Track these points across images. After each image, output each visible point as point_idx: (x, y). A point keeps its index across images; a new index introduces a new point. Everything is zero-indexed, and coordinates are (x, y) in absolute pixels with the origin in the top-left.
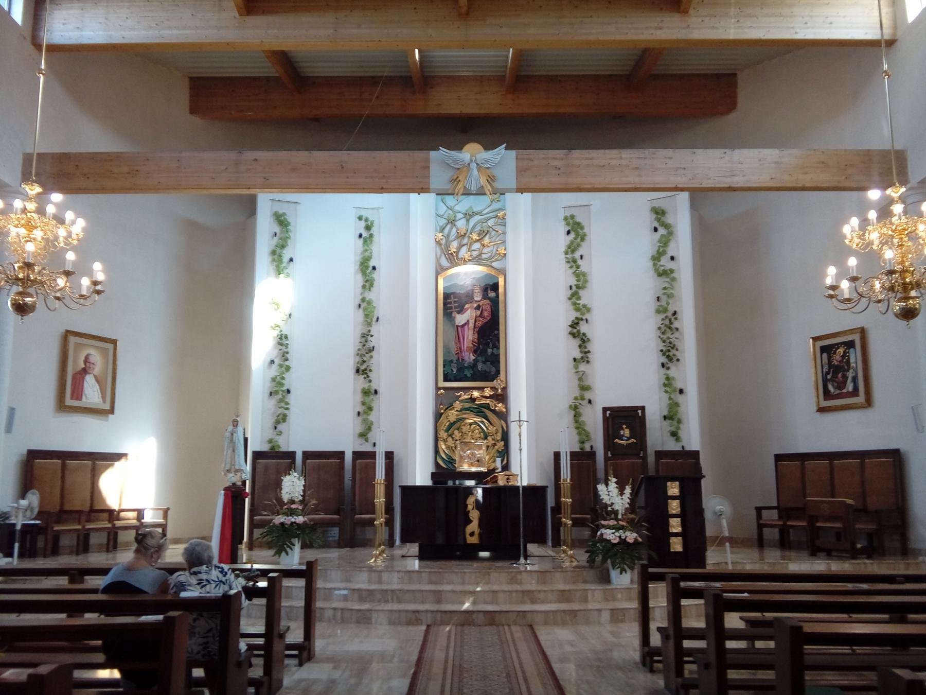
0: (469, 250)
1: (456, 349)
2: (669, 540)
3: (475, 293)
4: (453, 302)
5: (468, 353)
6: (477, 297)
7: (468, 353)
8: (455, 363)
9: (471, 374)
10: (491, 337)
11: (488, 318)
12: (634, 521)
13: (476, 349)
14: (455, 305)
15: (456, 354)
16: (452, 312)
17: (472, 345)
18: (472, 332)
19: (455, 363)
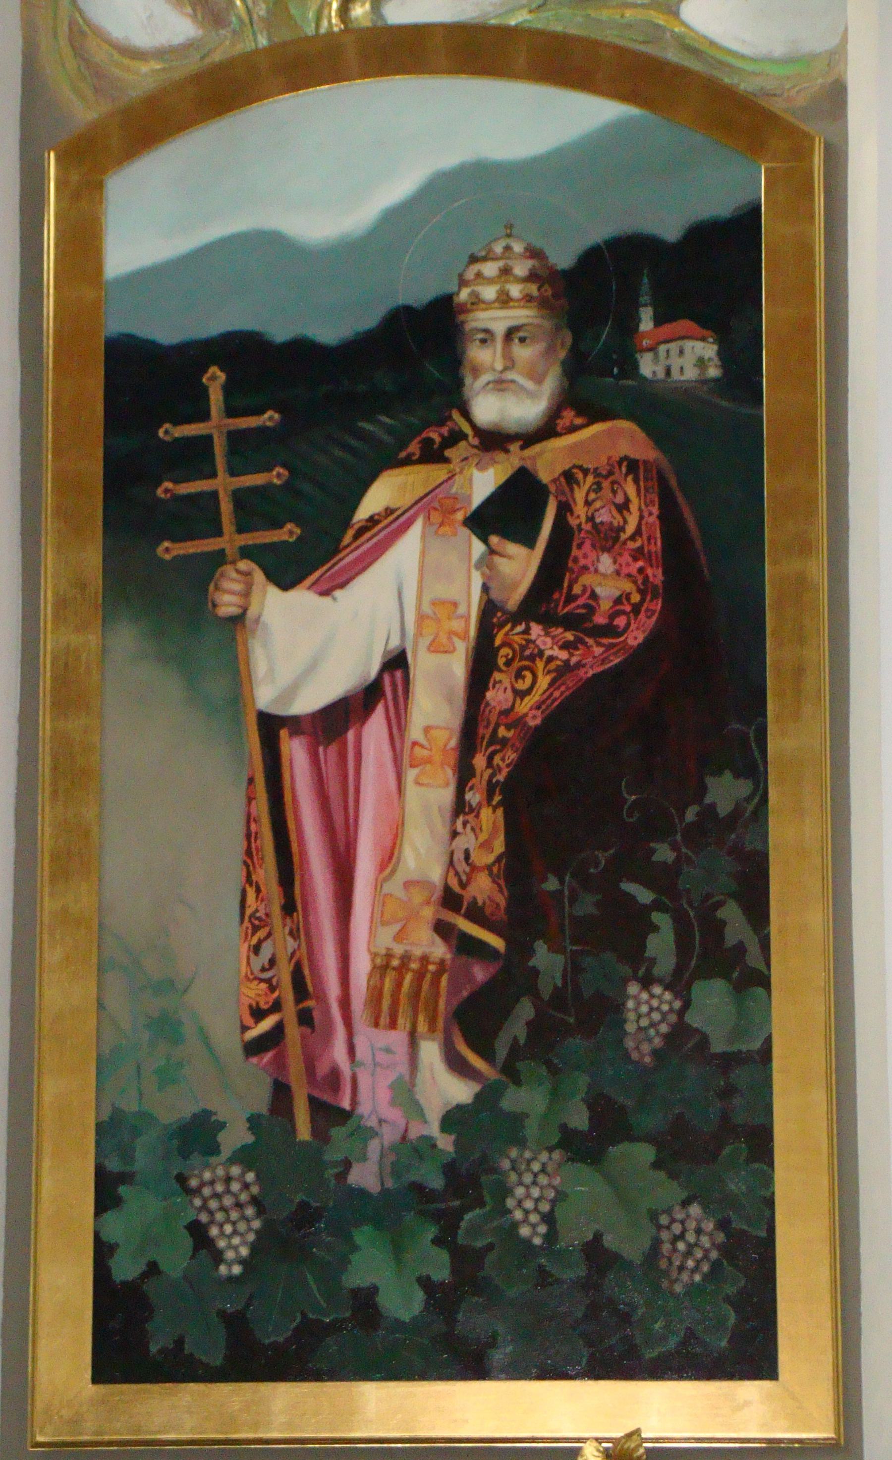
0: (453, 476)
1: (255, 992)
2: (501, 1109)
3: (487, 337)
4: (226, 507)
5: (398, 1039)
6: (500, 385)
7: (398, 1039)
8: (244, 1157)
9: (426, 1283)
10: (664, 853)
11: (636, 637)
12: (840, 1444)
13: (490, 985)
14: (216, 398)
15: (254, 1048)
16: (219, 559)
17: (439, 950)
18: (446, 795)
19: (244, 1157)
